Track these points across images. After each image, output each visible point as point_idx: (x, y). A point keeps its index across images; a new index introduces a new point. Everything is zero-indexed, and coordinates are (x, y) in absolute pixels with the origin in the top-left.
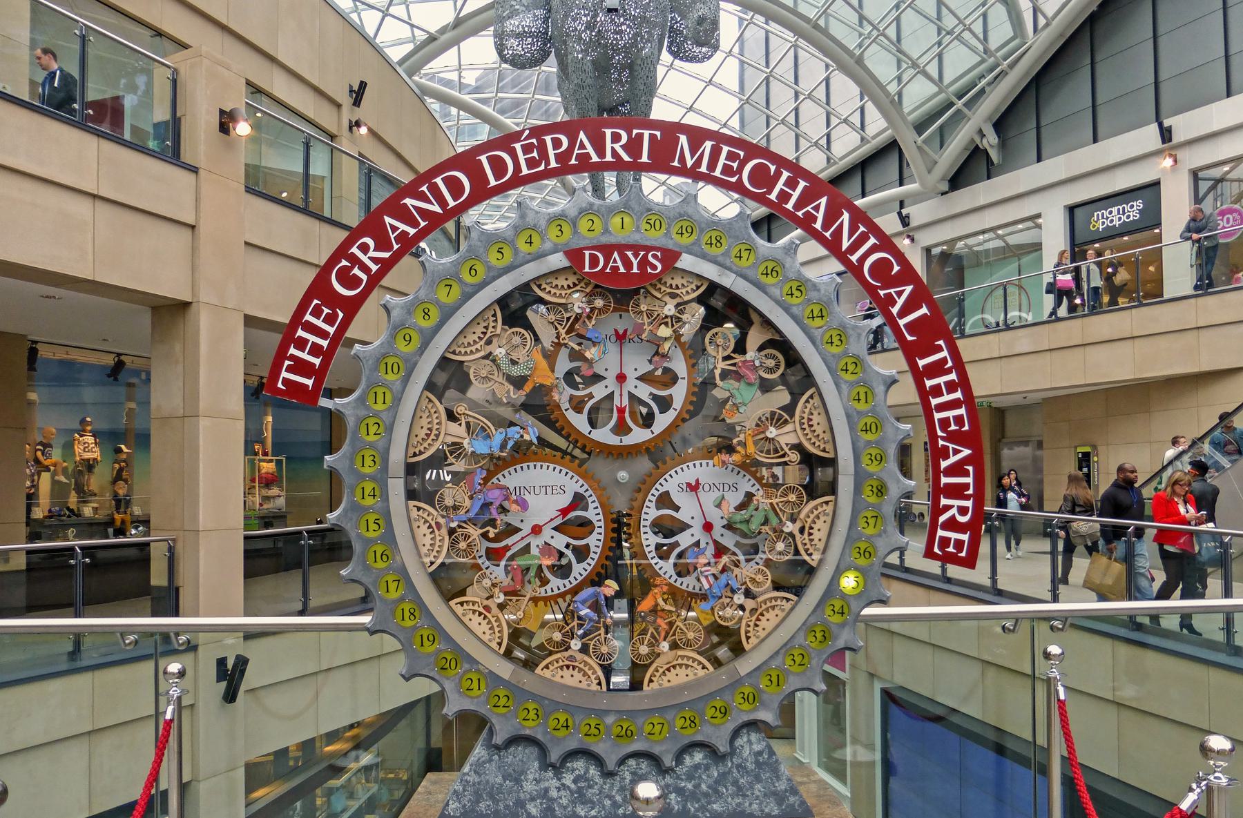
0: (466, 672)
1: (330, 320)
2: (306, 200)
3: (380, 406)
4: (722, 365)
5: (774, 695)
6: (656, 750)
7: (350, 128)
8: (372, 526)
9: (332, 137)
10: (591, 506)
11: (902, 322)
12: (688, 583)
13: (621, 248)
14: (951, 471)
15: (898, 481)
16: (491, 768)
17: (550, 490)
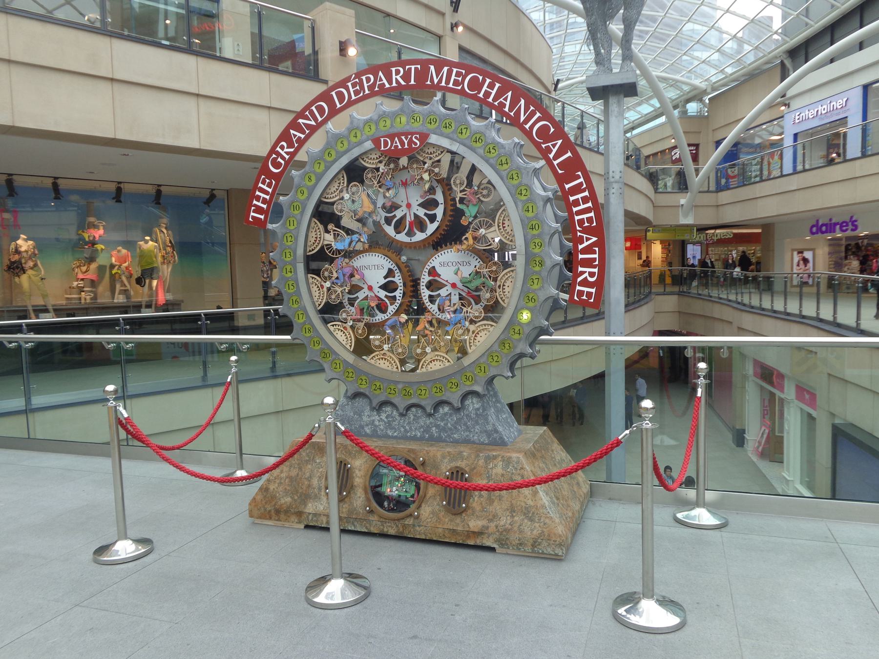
0: (333, 360)
1: (269, 186)
2: (734, 13)
3: (292, 228)
4: (459, 195)
5: (483, 377)
6: (423, 403)
7: (452, 29)
8: (291, 287)
9: (440, 37)
10: (397, 275)
11: (555, 163)
12: (443, 317)
13: (399, 135)
14: (584, 251)
15: (551, 257)
16: (348, 408)
17: (377, 267)
